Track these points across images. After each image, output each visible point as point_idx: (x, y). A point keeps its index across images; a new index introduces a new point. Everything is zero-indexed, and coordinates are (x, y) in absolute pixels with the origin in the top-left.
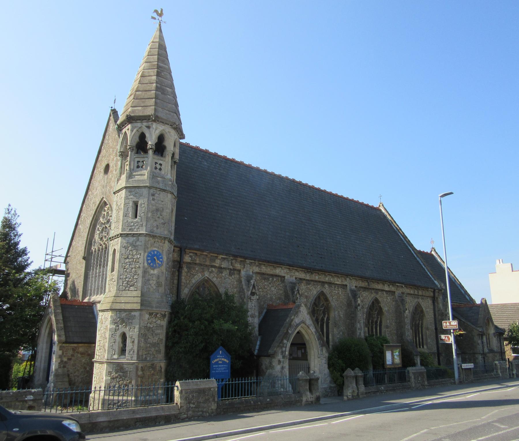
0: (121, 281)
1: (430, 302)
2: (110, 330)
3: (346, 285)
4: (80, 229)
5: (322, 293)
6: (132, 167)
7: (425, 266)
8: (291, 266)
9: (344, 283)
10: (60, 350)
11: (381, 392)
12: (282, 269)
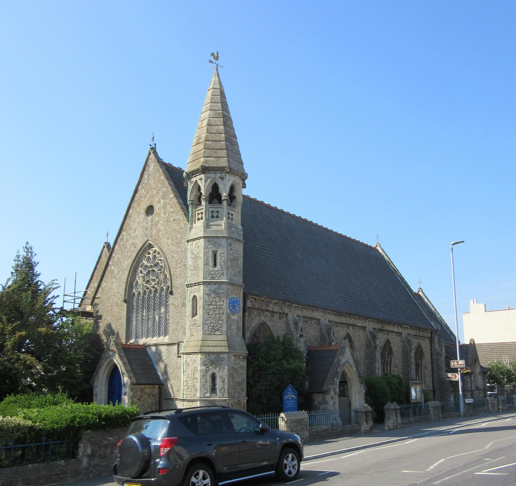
0: (206, 326)
1: (428, 342)
2: (201, 371)
3: (366, 327)
4: (112, 271)
5: (263, 324)
6: (207, 217)
8: (325, 310)
9: (364, 325)
10: (131, 391)
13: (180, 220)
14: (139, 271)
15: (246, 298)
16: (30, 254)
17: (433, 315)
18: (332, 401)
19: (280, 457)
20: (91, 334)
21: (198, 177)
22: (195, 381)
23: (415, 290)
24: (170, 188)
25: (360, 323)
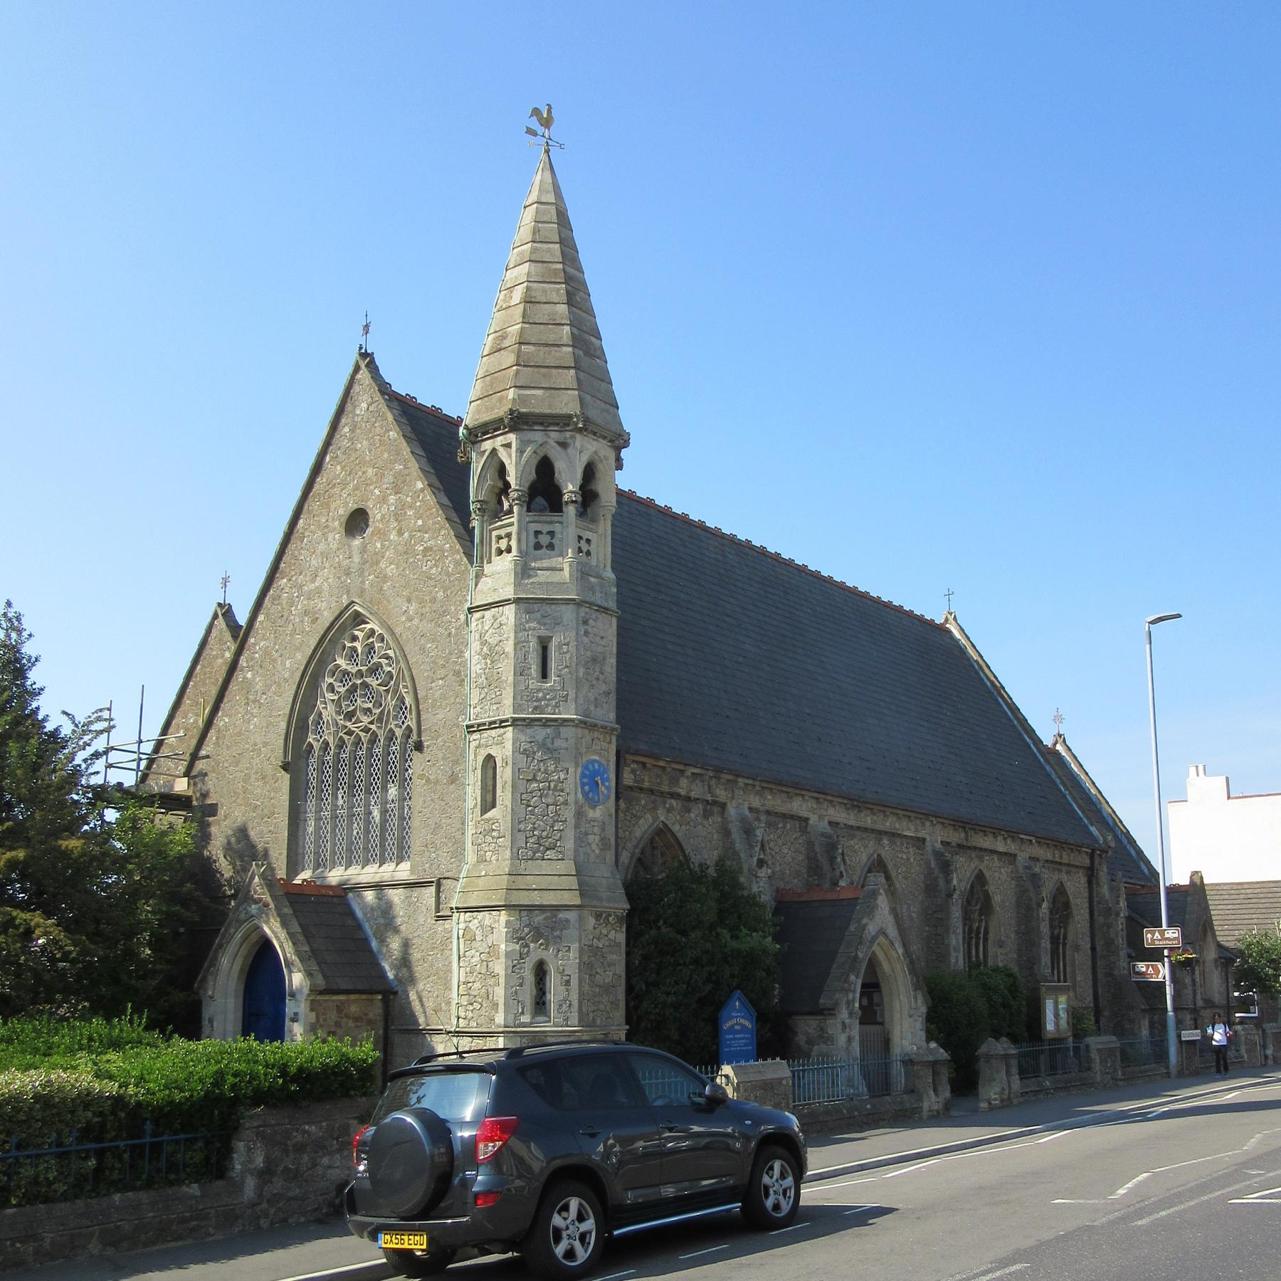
0: (521, 837)
1: (1084, 880)
2: (507, 954)
3: (924, 840)
4: (248, 686)
5: (663, 832)
7: (1066, 788)
8: (822, 793)
9: (920, 835)
10: (312, 1010)
12: (804, 800)
13: (443, 551)
14: (325, 687)
15: (622, 760)
16: (14, 635)
17: (1094, 808)
18: (844, 1034)
19: (752, 1172)
20: (191, 855)
21: (500, 440)
22: (492, 981)
23: (1048, 741)
24: (414, 466)
25: (909, 829)
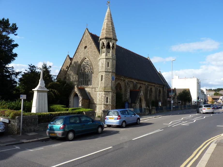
5: (119, 83)
11: (158, 112)
18: (138, 105)
23: (158, 72)
